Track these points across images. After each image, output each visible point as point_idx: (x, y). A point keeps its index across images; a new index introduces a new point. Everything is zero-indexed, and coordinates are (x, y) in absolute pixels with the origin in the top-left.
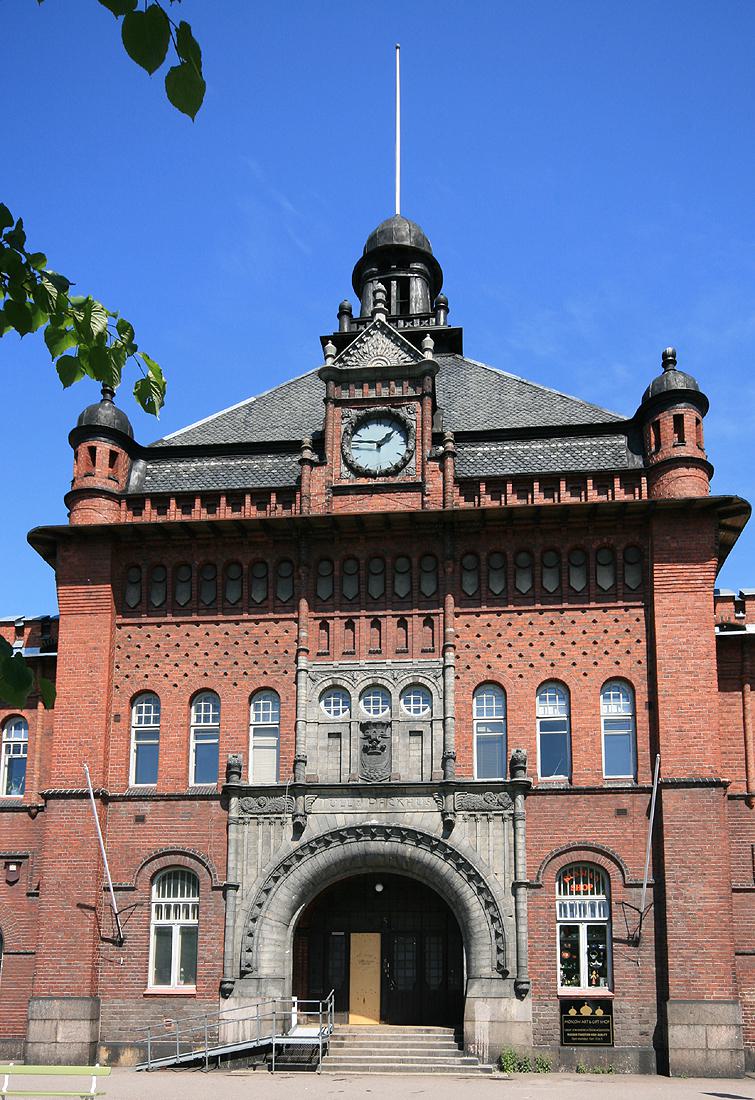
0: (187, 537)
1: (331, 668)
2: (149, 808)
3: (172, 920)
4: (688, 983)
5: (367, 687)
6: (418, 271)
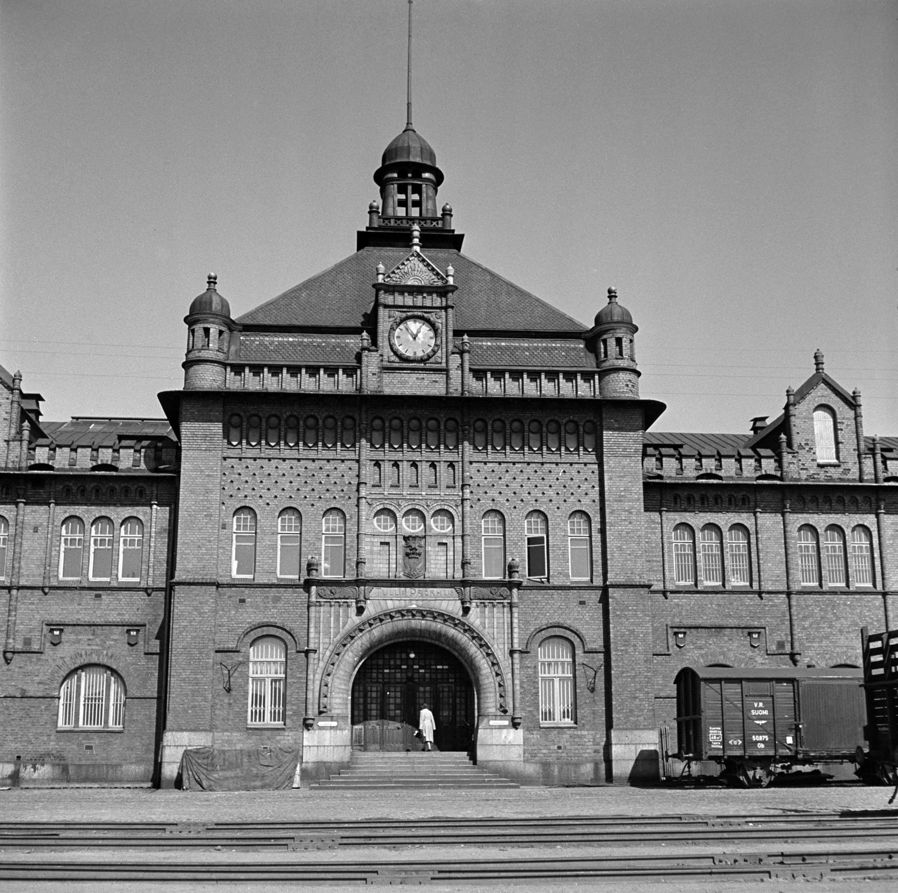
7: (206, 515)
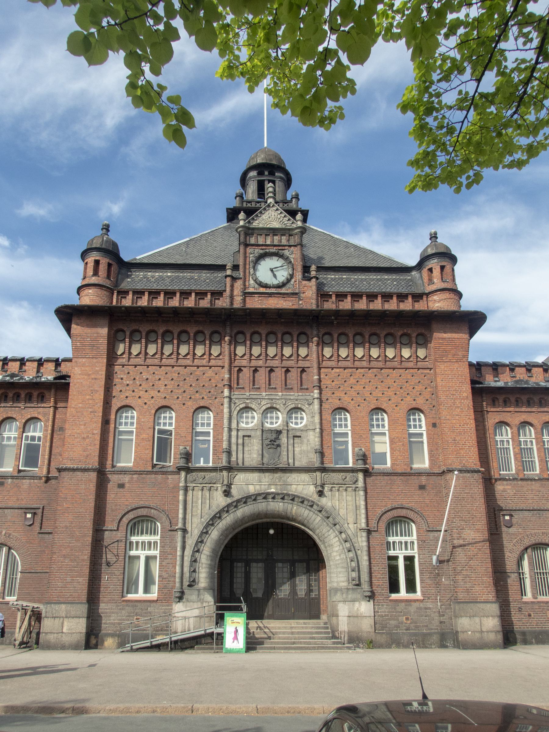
0: (157, 315)
1: (245, 396)
2: (127, 479)
3: (398, 551)
4: (468, 591)
5: (267, 409)
6: (281, 178)
7: (91, 412)
